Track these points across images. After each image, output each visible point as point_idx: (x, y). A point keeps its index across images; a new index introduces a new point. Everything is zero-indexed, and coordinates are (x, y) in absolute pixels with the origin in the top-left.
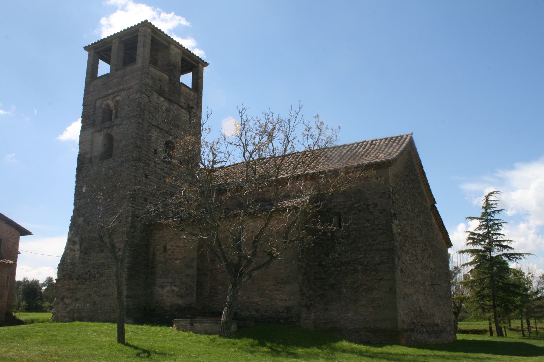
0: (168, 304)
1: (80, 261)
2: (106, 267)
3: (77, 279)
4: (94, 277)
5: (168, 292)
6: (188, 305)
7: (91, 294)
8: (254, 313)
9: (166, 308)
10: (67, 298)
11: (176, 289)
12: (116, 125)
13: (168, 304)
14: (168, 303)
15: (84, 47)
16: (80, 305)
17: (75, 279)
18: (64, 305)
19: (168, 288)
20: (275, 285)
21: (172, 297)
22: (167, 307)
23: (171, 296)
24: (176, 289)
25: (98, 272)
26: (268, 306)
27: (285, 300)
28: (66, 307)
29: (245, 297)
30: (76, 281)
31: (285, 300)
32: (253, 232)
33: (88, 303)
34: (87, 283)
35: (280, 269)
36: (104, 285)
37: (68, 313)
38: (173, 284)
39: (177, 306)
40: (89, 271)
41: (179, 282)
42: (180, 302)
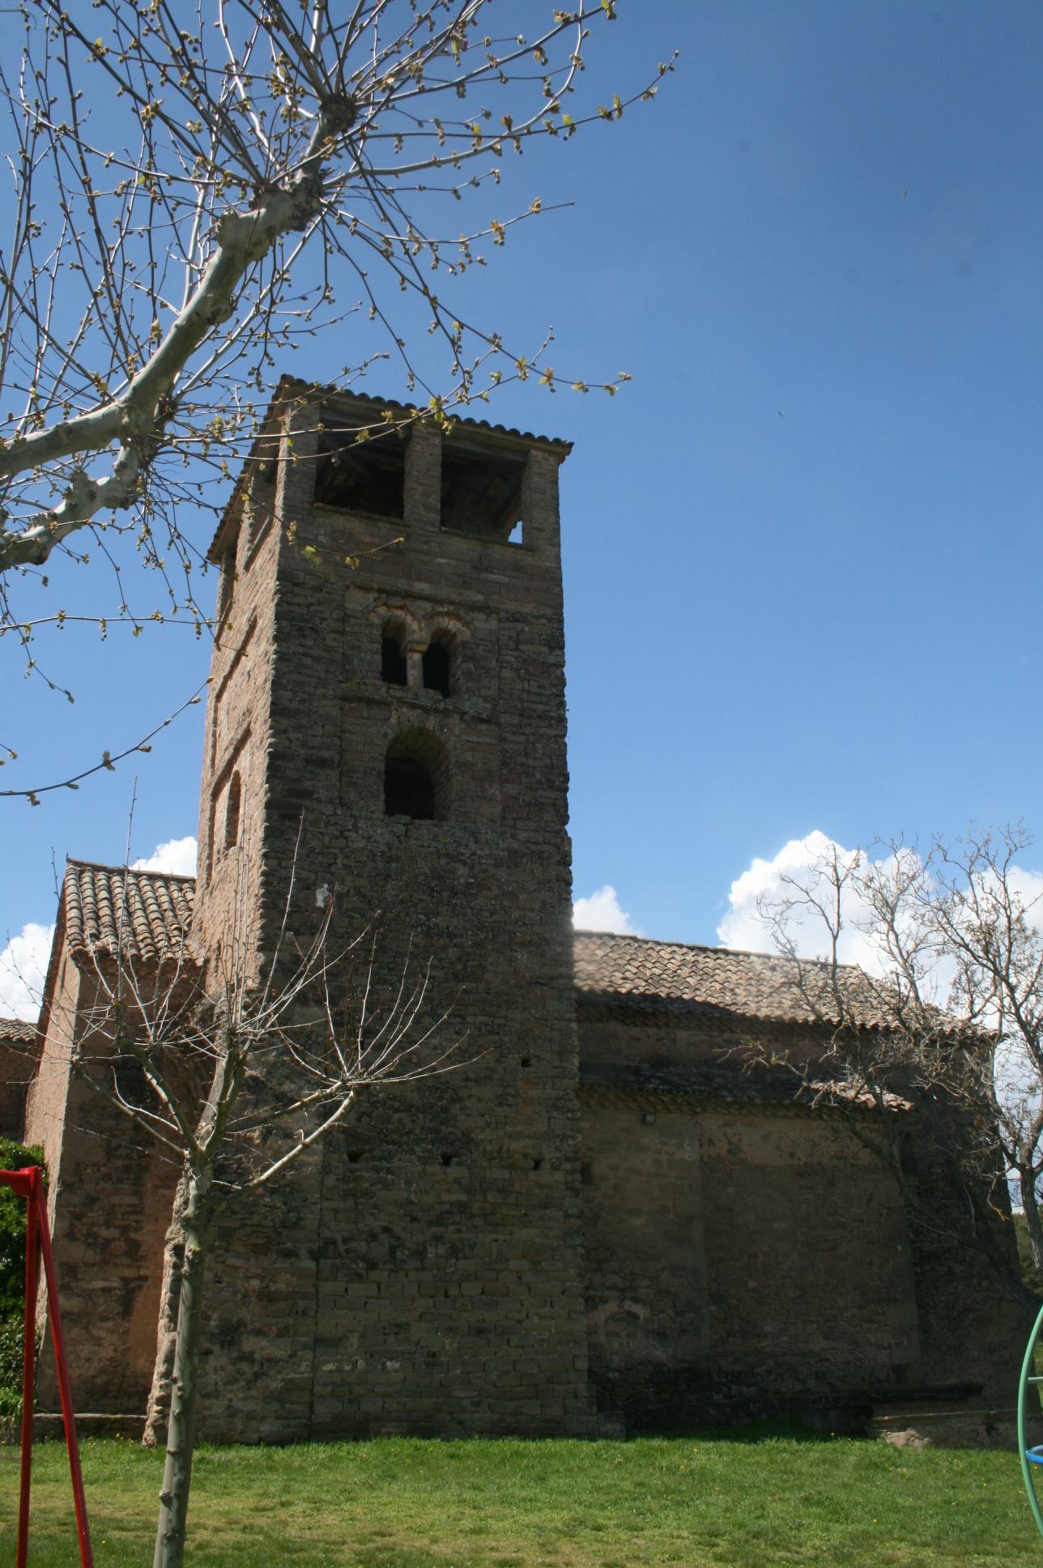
0: (616, 1361)
1: (330, 1181)
2: (479, 1222)
3: (316, 1256)
4: (420, 1254)
5: (612, 1317)
6: (686, 1365)
7: (408, 1324)
8: (812, 1383)
9: (611, 1375)
10: (258, 1333)
11: (641, 1311)
12: (462, 714)
13: (616, 1361)
14: (616, 1359)
15: (560, 449)
16: (347, 1368)
17: (303, 1253)
18: (244, 1366)
19: (612, 1307)
20: (860, 1307)
21: (628, 1336)
22: (615, 1370)
23: (623, 1334)
24: (641, 1311)
25: (438, 1239)
26: (848, 1363)
27: (890, 1347)
28: (257, 1376)
29: (784, 1338)
30: (310, 1264)
31: (890, 1347)
32: (792, 1155)
33: (391, 1359)
34: (374, 1275)
35: (871, 1264)
36: (471, 1289)
37: (279, 1397)
38: (629, 1294)
39: (651, 1368)
40: (387, 1230)
41: (648, 1287)
42: (661, 1354)
